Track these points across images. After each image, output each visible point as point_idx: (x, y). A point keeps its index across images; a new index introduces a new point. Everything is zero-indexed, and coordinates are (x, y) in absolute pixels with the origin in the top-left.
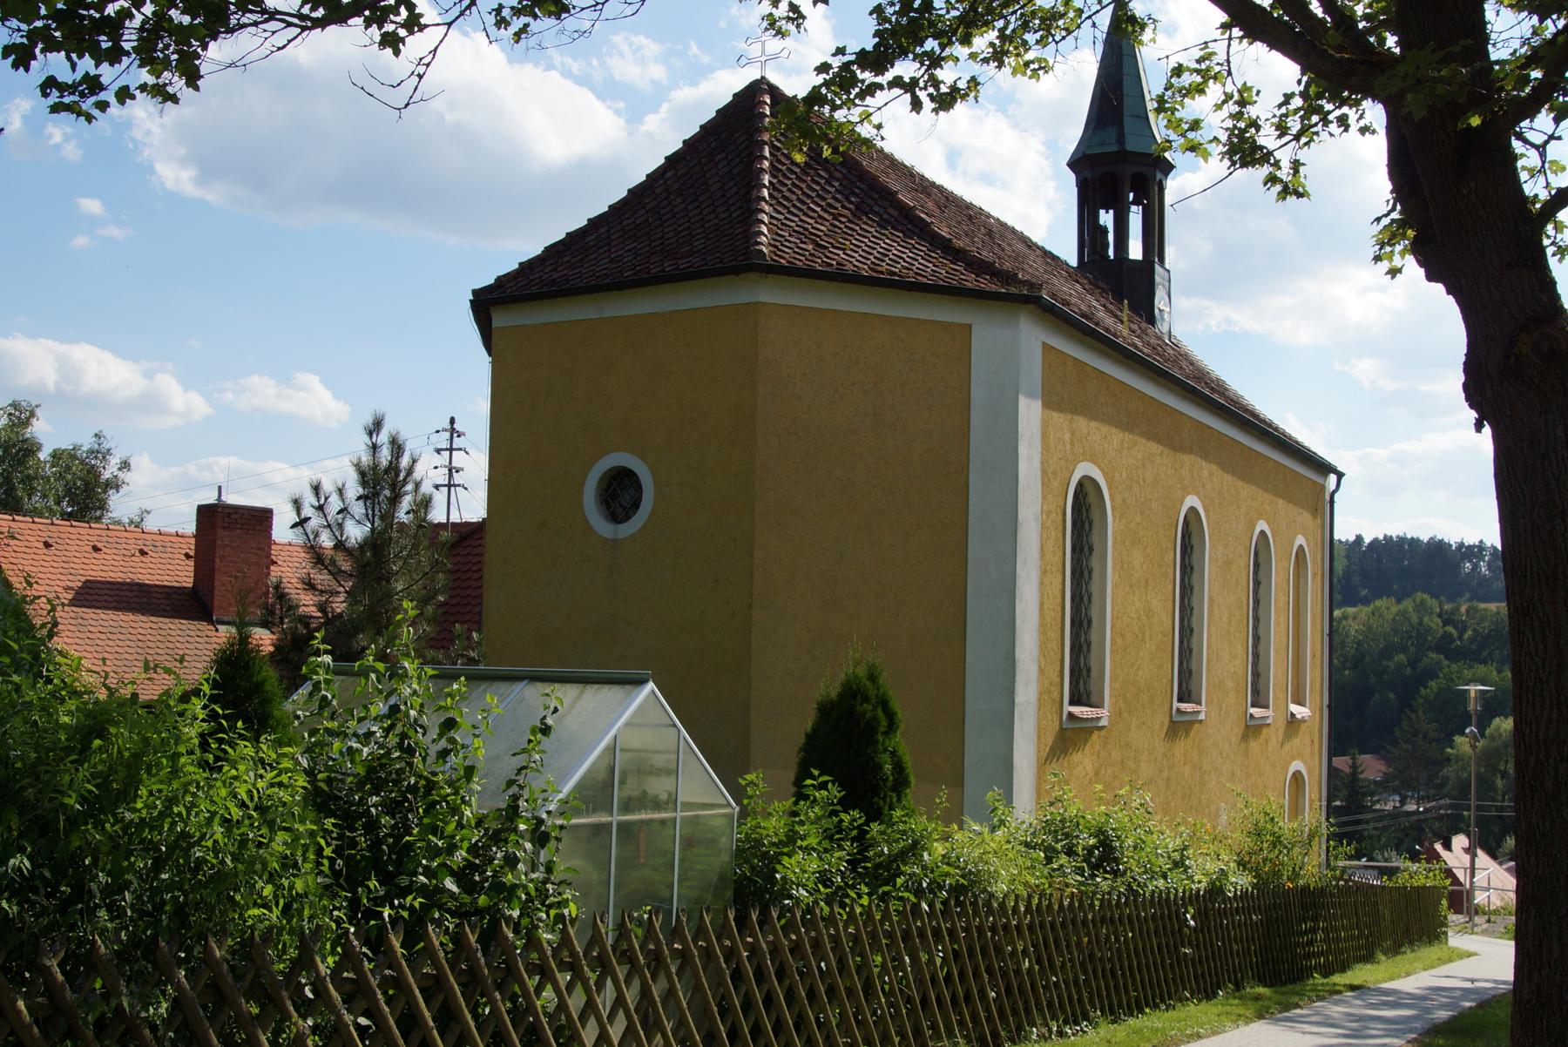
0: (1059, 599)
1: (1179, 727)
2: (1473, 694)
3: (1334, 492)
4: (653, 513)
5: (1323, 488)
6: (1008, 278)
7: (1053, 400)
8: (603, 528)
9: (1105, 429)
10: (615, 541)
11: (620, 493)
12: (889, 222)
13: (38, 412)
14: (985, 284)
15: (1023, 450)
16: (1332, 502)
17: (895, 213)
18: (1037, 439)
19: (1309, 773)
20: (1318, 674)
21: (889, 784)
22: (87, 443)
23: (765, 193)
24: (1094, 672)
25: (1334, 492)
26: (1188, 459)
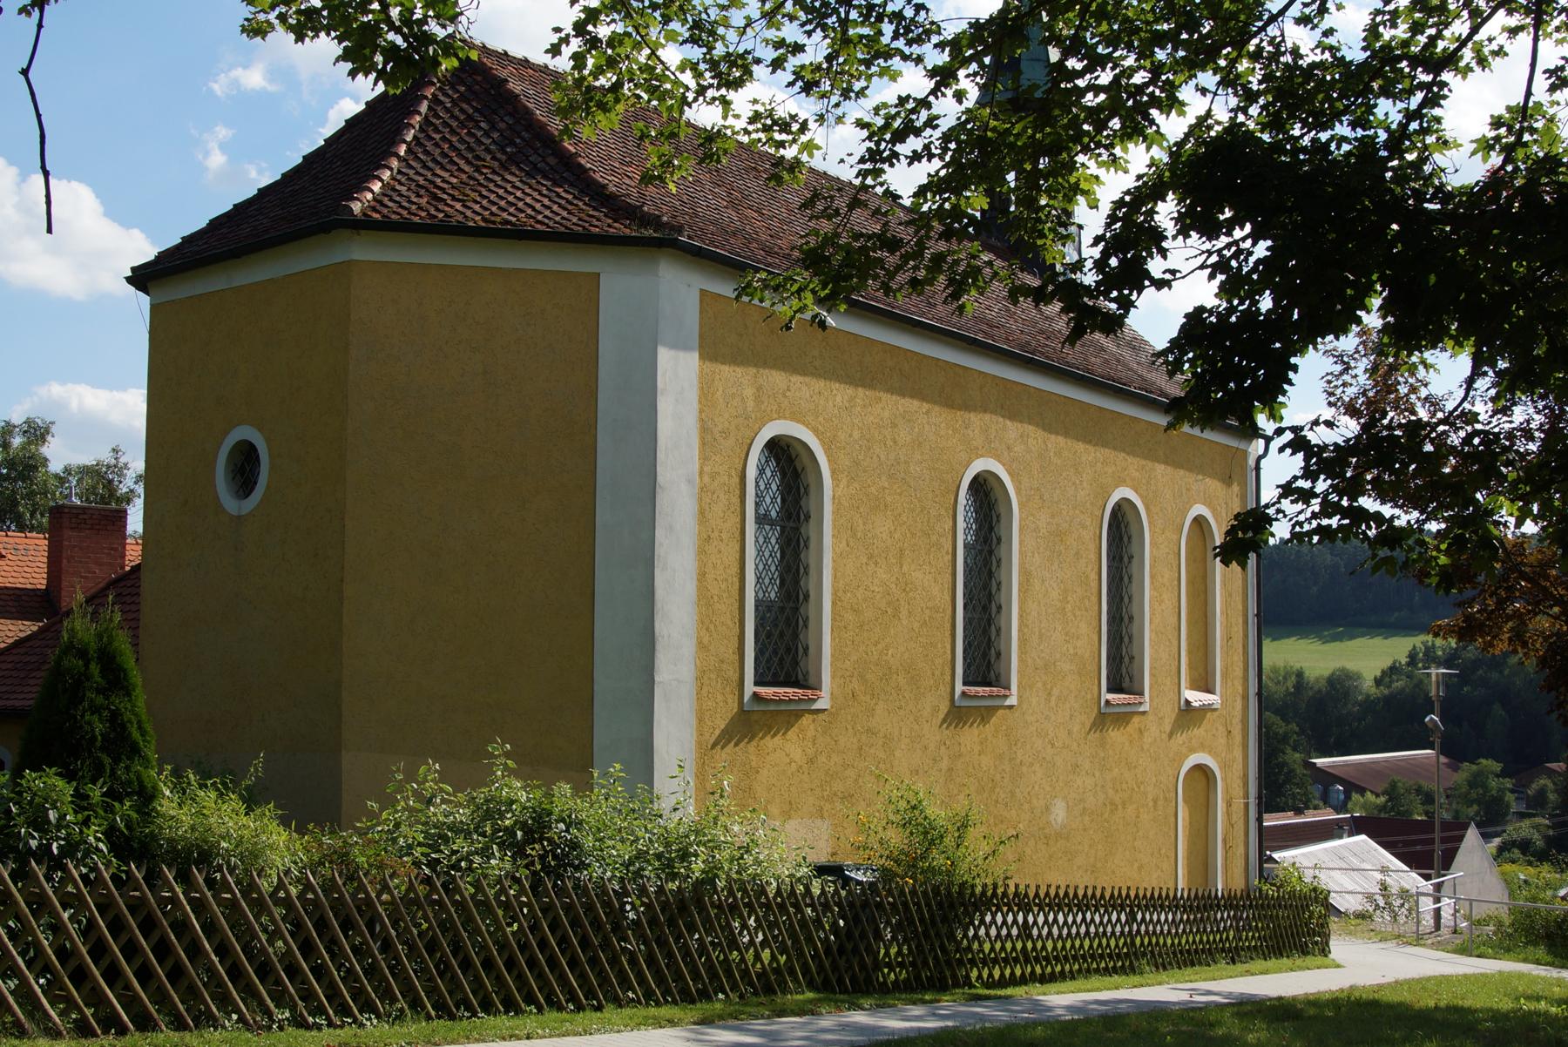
0: (735, 569)
1: (1106, 719)
2: (1434, 678)
3: (1260, 458)
4: (268, 487)
5: (1245, 453)
6: (653, 221)
7: (713, 349)
8: (230, 504)
9: (820, 384)
10: (239, 517)
11: (245, 465)
12: (540, 171)
13: (53, 429)
14: (602, 223)
15: (665, 406)
16: (1258, 468)
17: (552, 161)
18: (692, 396)
19: (1224, 766)
20: (1238, 659)
21: (98, 744)
22: (106, 457)
23: (402, 150)
24: (812, 651)
25: (1260, 458)
26: (975, 419)
